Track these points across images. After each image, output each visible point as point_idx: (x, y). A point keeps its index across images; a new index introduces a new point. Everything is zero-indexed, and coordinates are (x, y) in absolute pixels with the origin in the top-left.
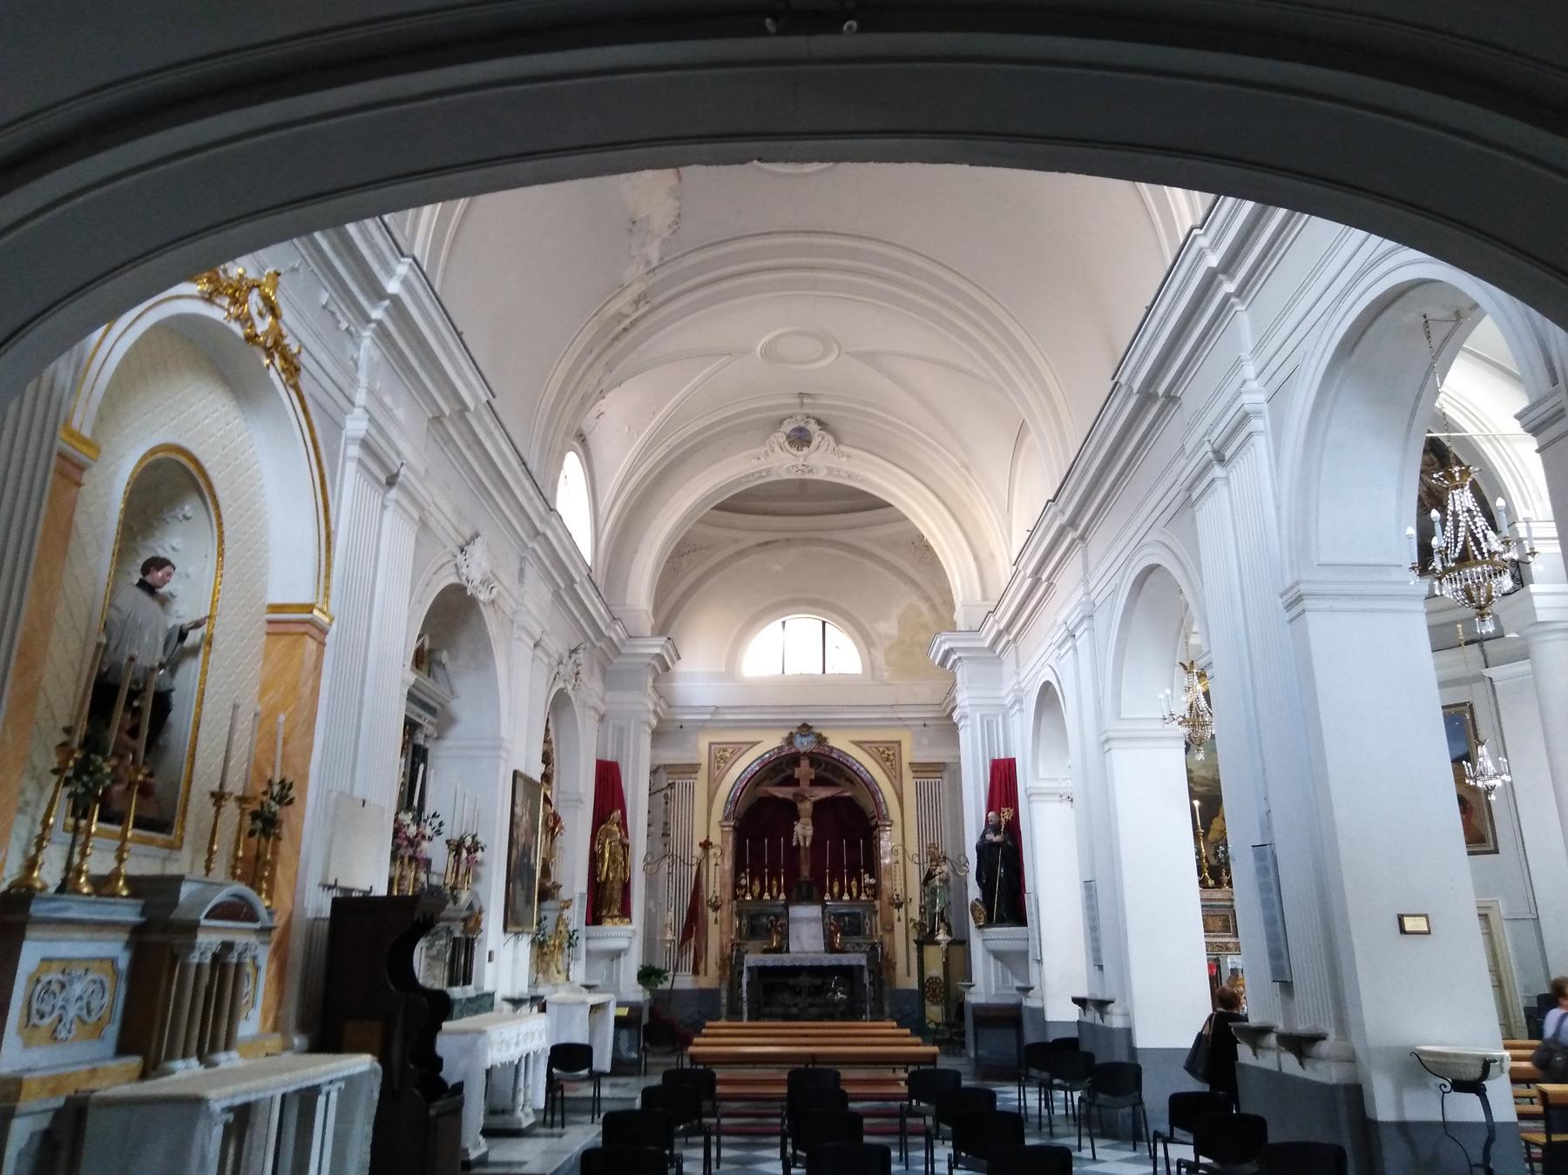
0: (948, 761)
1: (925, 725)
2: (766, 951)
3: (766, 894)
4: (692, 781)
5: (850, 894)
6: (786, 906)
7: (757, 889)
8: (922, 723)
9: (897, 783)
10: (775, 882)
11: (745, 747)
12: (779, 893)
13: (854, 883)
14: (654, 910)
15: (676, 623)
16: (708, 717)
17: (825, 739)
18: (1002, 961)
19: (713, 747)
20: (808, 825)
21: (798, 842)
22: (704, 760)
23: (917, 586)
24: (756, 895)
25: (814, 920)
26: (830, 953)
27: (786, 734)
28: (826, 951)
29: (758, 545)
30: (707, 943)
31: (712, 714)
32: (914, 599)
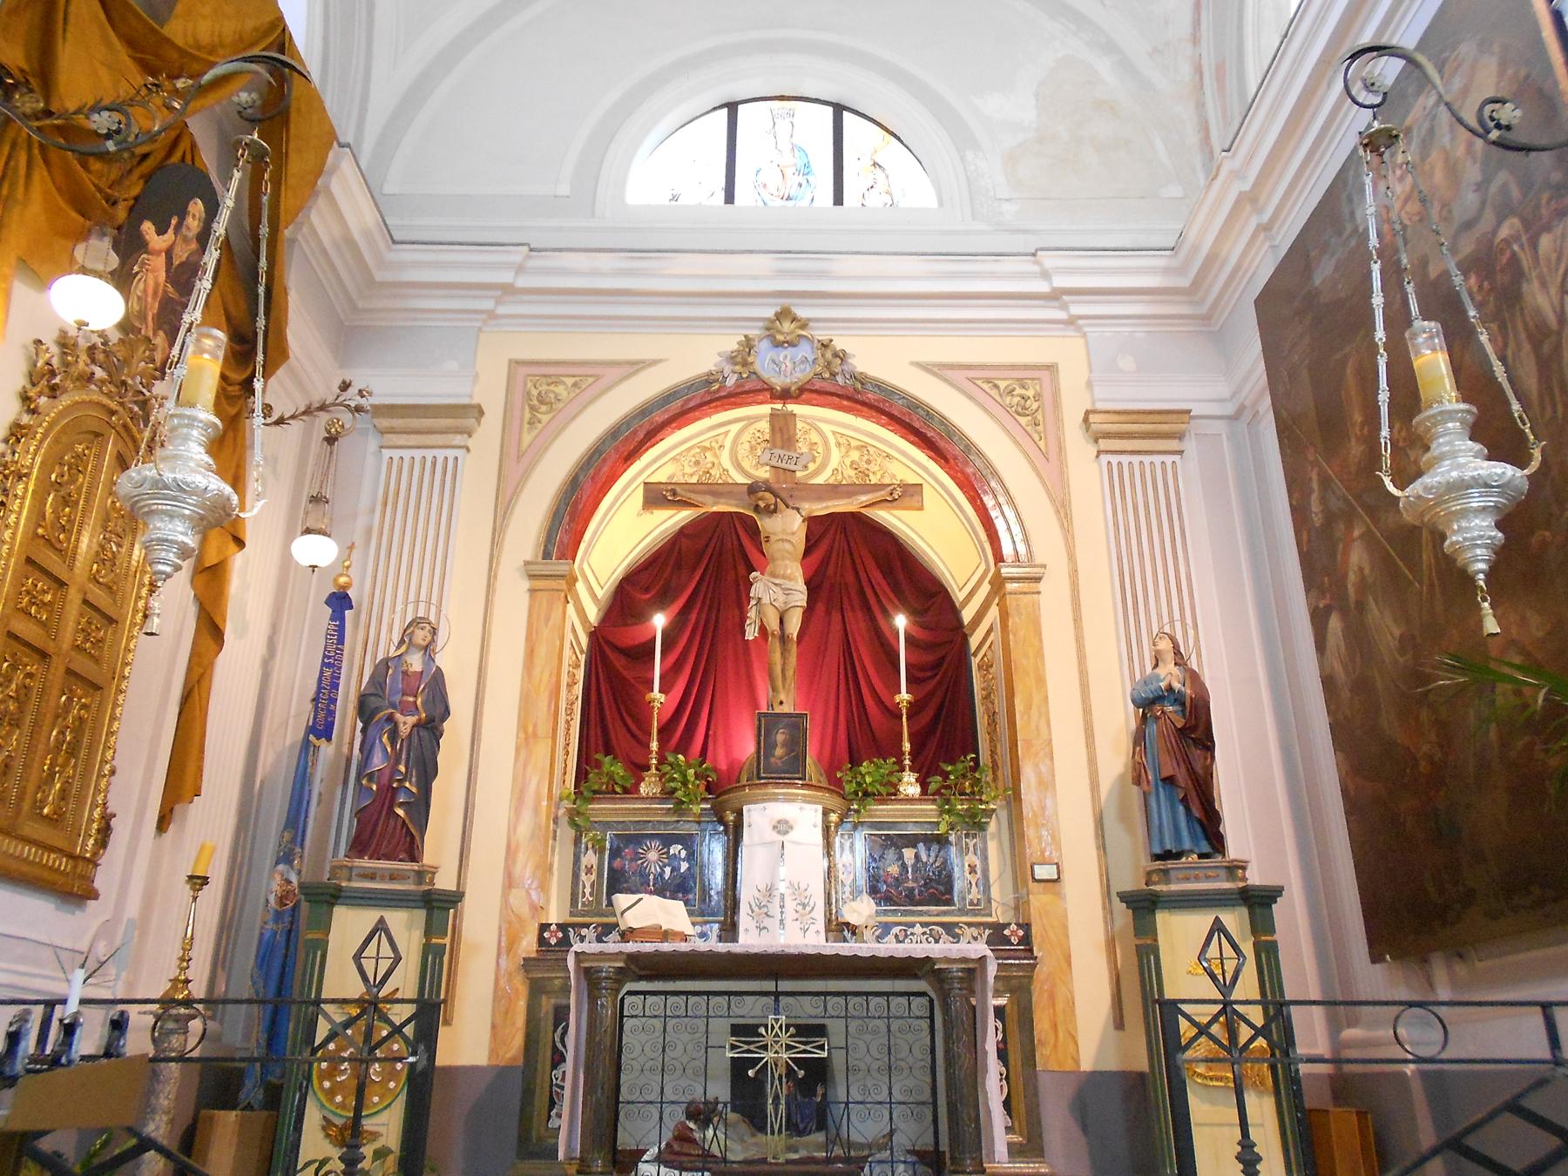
4: (451, 453)
17: (842, 356)
27: (731, 343)
30: (324, 957)
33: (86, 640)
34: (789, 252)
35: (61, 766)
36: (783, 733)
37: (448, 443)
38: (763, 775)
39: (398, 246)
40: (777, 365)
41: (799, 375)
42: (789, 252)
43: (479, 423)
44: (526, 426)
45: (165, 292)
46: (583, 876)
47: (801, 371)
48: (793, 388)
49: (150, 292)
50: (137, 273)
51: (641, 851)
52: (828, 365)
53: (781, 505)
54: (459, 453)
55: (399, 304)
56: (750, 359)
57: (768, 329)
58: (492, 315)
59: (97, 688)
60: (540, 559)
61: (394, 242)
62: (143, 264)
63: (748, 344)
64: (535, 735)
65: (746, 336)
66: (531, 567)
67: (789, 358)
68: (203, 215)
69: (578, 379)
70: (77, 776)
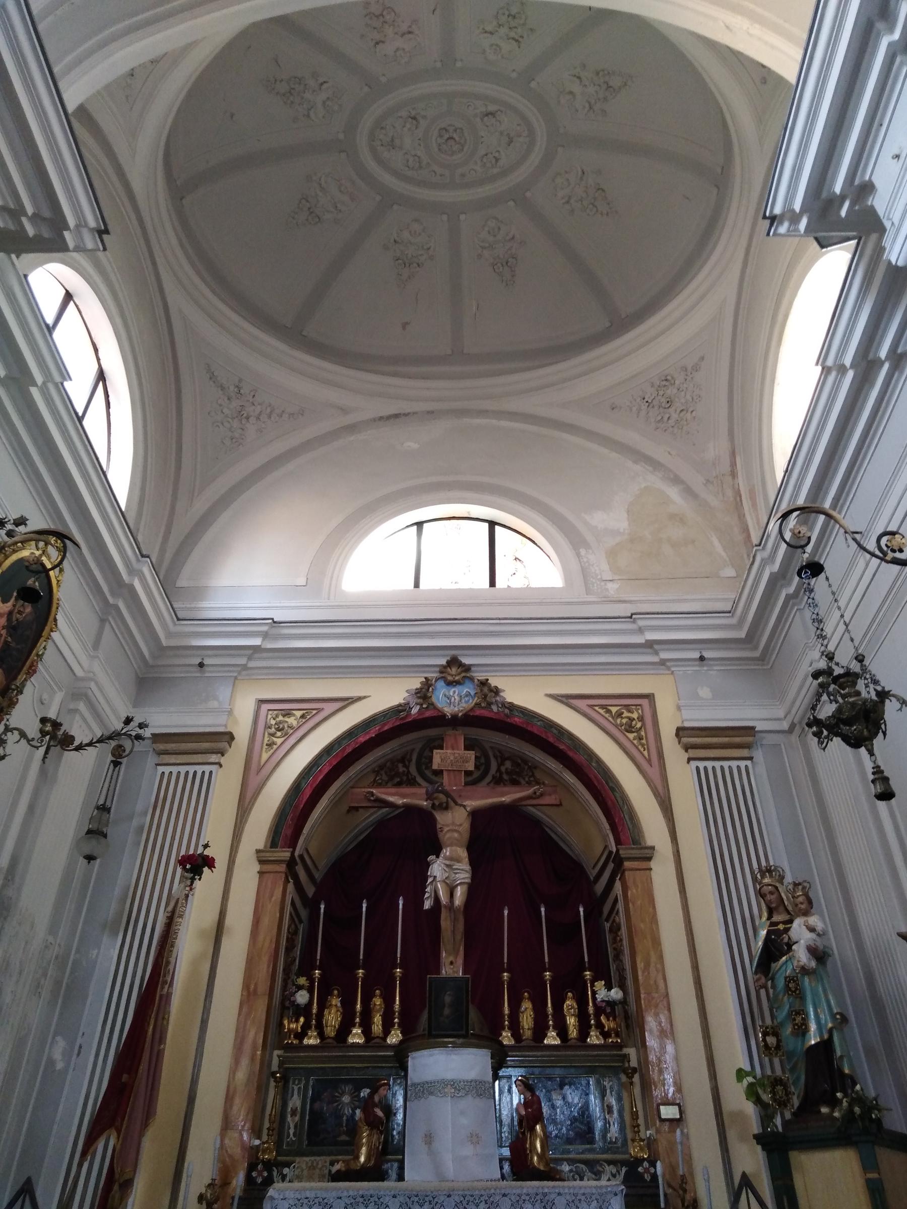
0: (760, 726)
1: (702, 658)
2: (337, 1177)
3: (357, 1031)
4: (207, 769)
5: (562, 1032)
7: (332, 1019)
8: (696, 655)
9: (654, 772)
10: (378, 1001)
11: (329, 708)
12: (387, 1028)
13: (570, 1003)
14: (60, 1066)
15: (224, 517)
16: (257, 641)
17: (496, 691)
19: (265, 707)
20: (459, 860)
21: (437, 899)
22: (242, 732)
23: (655, 464)
24: (330, 1032)
27: (415, 683)
29: (381, 418)
31: (265, 636)
32: (654, 480)
37: (205, 761)
38: (434, 1033)
41: (464, 705)
46: (289, 1119)
47: (466, 702)
48: (460, 714)
51: (337, 1094)
53: (452, 804)
54: (214, 768)
57: (441, 672)
58: (245, 667)
61: (178, 619)
67: (457, 693)
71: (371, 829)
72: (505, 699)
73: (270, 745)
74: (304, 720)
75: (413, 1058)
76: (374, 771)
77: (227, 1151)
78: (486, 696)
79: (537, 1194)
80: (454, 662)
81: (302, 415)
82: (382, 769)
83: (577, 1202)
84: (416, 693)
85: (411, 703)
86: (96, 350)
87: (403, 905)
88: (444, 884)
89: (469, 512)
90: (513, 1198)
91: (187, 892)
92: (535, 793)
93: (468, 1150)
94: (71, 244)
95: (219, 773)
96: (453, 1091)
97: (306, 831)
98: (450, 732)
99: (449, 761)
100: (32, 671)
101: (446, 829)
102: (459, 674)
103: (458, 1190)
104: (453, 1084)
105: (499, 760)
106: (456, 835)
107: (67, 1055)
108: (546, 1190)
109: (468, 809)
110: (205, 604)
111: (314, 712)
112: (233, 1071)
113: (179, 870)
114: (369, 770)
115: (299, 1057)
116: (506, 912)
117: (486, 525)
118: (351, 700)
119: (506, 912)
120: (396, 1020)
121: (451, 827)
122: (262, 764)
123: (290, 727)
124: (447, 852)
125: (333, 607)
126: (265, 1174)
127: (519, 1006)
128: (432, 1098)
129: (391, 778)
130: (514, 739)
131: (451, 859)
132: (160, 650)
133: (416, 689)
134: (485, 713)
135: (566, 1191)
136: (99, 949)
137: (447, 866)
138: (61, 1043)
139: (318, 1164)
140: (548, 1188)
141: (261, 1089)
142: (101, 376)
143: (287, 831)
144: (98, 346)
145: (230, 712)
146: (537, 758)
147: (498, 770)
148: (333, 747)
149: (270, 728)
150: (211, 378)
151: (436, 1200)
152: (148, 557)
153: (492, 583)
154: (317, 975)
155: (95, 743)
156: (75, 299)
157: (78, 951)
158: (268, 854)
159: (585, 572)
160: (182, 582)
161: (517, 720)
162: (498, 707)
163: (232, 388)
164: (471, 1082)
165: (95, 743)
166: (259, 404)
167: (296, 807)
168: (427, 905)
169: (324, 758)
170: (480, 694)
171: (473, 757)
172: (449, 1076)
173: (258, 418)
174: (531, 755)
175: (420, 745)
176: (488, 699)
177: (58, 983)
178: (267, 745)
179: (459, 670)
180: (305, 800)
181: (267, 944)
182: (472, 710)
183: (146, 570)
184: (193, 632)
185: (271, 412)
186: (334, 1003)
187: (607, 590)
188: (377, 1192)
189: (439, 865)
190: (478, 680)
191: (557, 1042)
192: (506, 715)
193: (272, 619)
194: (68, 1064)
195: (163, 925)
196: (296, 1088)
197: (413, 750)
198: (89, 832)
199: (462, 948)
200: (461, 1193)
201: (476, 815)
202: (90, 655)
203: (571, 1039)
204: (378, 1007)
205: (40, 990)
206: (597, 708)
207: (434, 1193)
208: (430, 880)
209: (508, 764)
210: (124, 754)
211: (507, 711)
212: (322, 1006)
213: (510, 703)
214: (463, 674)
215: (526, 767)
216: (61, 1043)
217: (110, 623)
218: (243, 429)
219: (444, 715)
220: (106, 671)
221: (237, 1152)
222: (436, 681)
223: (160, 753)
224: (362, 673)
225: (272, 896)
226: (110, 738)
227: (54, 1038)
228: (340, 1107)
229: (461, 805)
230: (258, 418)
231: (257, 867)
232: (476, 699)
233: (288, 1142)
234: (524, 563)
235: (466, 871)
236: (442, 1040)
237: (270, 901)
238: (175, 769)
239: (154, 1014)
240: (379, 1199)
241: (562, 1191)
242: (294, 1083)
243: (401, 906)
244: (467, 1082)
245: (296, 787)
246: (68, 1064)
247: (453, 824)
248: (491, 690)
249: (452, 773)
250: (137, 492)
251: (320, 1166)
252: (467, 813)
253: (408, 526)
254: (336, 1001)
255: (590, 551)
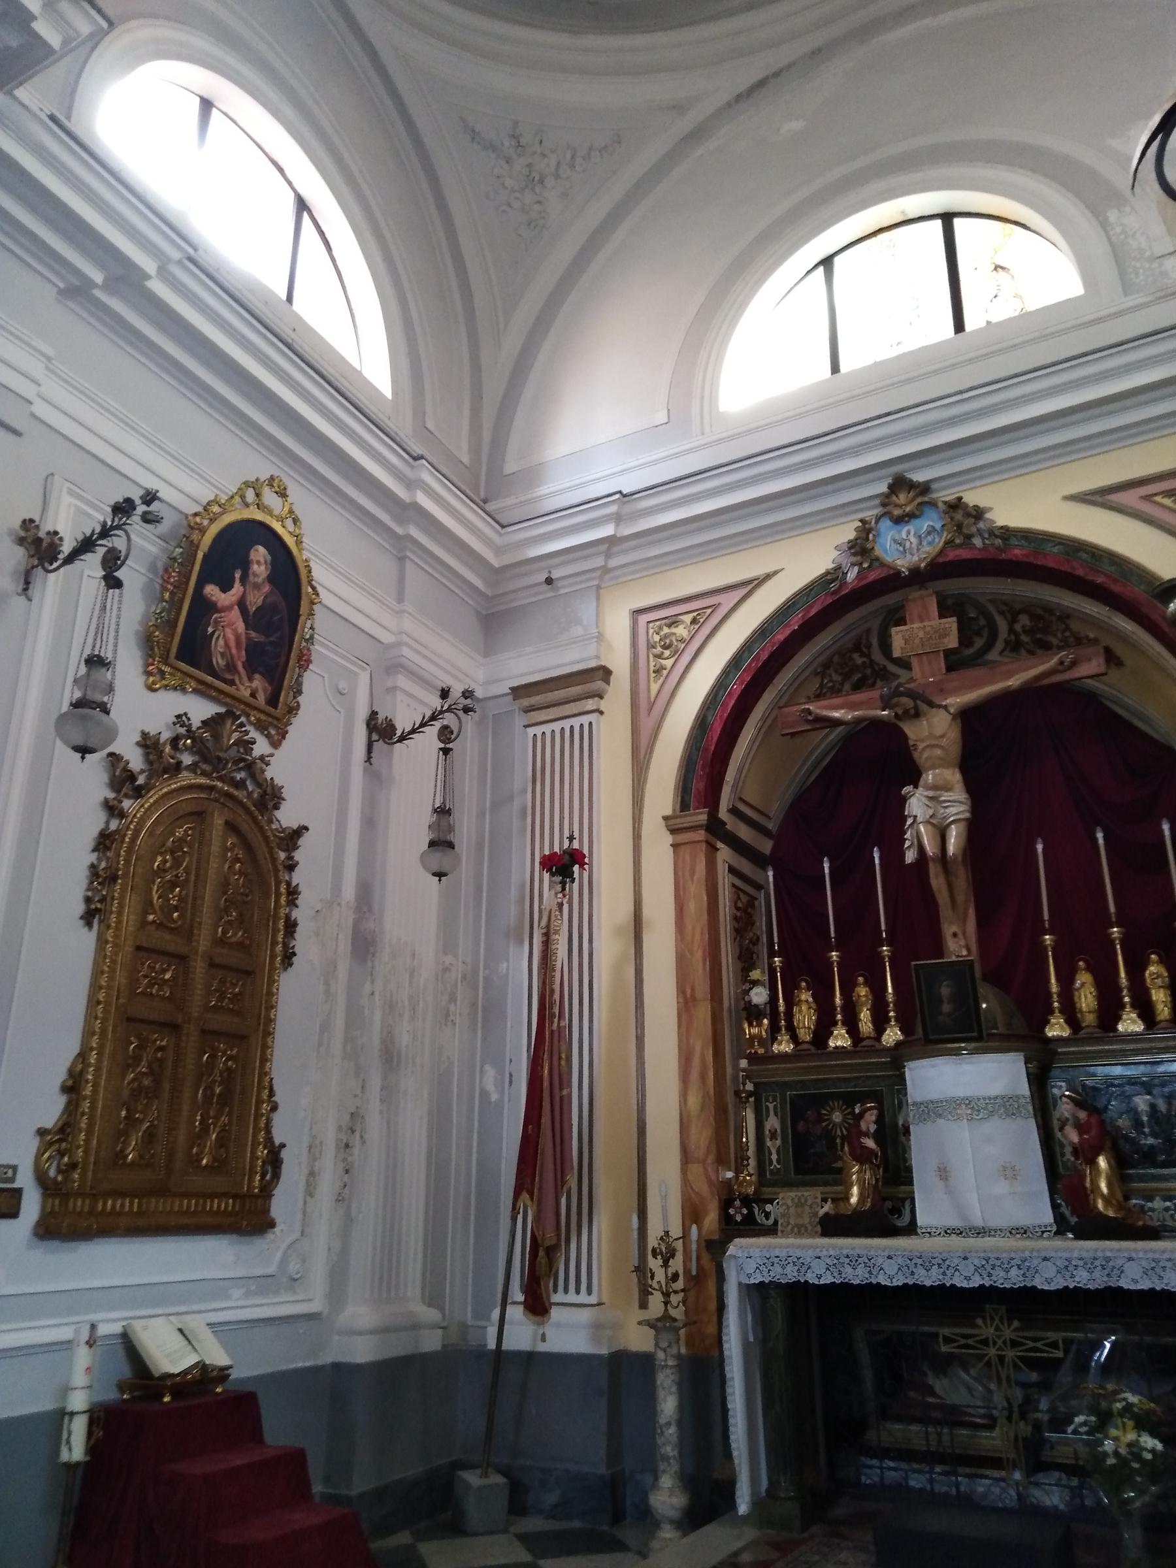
2: (833, 1226)
4: (585, 719)
6: (898, 1057)
7: (806, 1018)
10: (862, 991)
12: (880, 1024)
14: (494, 1097)
16: (608, 530)
17: (978, 514)
18: (106, 708)
19: (643, 619)
20: (947, 788)
21: (921, 849)
22: (619, 661)
24: (805, 1035)
25: (1003, 1106)
26: (1082, 1234)
27: (847, 532)
28: (1062, 1227)
29: (739, 98)
31: (618, 519)
33: (221, 998)
34: (888, 414)
35: (214, 1118)
36: (948, 986)
37: (581, 710)
38: (932, 1037)
39: (509, 529)
40: (900, 544)
41: (927, 549)
42: (888, 414)
43: (608, 683)
44: (653, 675)
45: (248, 639)
46: (769, 1143)
47: (930, 543)
48: (923, 565)
49: (232, 643)
50: (213, 633)
51: (824, 1112)
52: (959, 526)
53: (924, 707)
54: (592, 717)
55: (521, 583)
56: (869, 546)
57: (884, 505)
58: (605, 570)
59: (243, 1038)
60: (678, 813)
61: (503, 527)
62: (216, 623)
63: (866, 530)
64: (694, 999)
65: (861, 521)
66: (671, 822)
67: (912, 533)
68: (269, 558)
69: (695, 614)
70: (235, 1122)
71: (837, 749)
72: (993, 522)
73: (657, 672)
74: (697, 627)
75: (910, 1069)
76: (816, 673)
77: (692, 1188)
78: (959, 526)
79: (1095, 1259)
80: (900, 484)
81: (619, 143)
82: (828, 668)
83: (1158, 1270)
84: (850, 548)
85: (844, 566)
86: (281, 170)
87: (881, 858)
88: (930, 827)
89: (903, 212)
90: (1058, 1263)
91: (560, 900)
92: (1061, 663)
93: (1001, 1188)
94: (54, 40)
95: (602, 725)
96: (969, 1111)
97: (730, 776)
98: (915, 594)
99: (917, 641)
100: (305, 661)
101: (921, 746)
102: (913, 500)
103: (977, 1252)
104: (968, 1102)
105: (1009, 617)
106: (939, 752)
107: (499, 1084)
108: (1108, 1254)
109: (952, 710)
110: (543, 490)
111: (709, 611)
112: (684, 1096)
113: (546, 876)
114: (807, 673)
115: (768, 1070)
116: (1040, 847)
117: (938, 223)
118: (756, 582)
119: (1040, 847)
120: (892, 1014)
121: (928, 743)
122: (652, 700)
123: (682, 640)
124: (929, 777)
125: (720, 441)
126: (745, 1211)
127: (1072, 980)
128: (941, 1121)
129: (846, 677)
130: (1020, 581)
131: (935, 787)
132: (497, 574)
133: (849, 542)
134: (964, 554)
135: (1141, 1255)
136: (508, 961)
137: (931, 798)
138: (490, 1072)
139: (806, 1201)
140: (1111, 1250)
141: (721, 1112)
142: (302, 206)
143: (698, 785)
144: (281, 163)
145: (600, 637)
146: (1066, 603)
147: (1011, 631)
148: (741, 656)
149: (654, 647)
150: (473, 139)
151: (947, 1263)
152: (422, 457)
153: (959, 326)
154: (777, 964)
155: (418, 728)
156: (216, 103)
157: (486, 967)
158: (678, 821)
159: (1119, 255)
160: (510, 467)
161: (1018, 552)
162: (983, 538)
163: (506, 143)
164: (996, 1098)
165: (418, 728)
166: (552, 152)
167: (706, 750)
168: (910, 856)
169: (731, 675)
170: (950, 526)
171: (955, 626)
172: (961, 1092)
173: (557, 176)
174: (1057, 601)
175: (878, 621)
176: (965, 531)
177: (474, 1005)
178: (654, 672)
179: (912, 494)
180: (715, 739)
181: (697, 937)
182: (941, 552)
183: (428, 477)
184: (529, 539)
185: (573, 157)
186: (803, 997)
187: (1165, 274)
188: (865, 1252)
189: (919, 800)
190: (945, 503)
191: (1139, 1027)
192: (998, 548)
193: (620, 492)
194: (502, 1093)
195: (541, 944)
196: (771, 1106)
197: (868, 631)
198: (432, 844)
199: (972, 913)
200: (982, 1255)
201: (968, 717)
202: (392, 610)
203: (1161, 1021)
204: (864, 999)
205: (452, 1017)
206: (1158, 499)
207: (944, 1254)
208: (910, 821)
209: (1024, 620)
210: (453, 737)
211: (998, 542)
212: (790, 1002)
213: (1002, 527)
214: (919, 500)
215: (1054, 619)
216: (490, 1072)
217: (412, 561)
218: (539, 202)
219: (898, 573)
220: (424, 624)
221: (702, 1187)
222: (877, 521)
223: (528, 710)
224: (756, 539)
225: (693, 873)
226: (433, 718)
227: (482, 1067)
228: (830, 1127)
229: (940, 706)
230: (557, 176)
231: (669, 839)
232: (945, 534)
233: (771, 1171)
234: (1012, 271)
235: (961, 802)
236: (944, 1046)
237: (692, 880)
238: (547, 728)
239: (546, 1054)
240: (870, 1260)
241: (1134, 1255)
242: (767, 1100)
243: (877, 861)
244: (990, 1099)
245: (701, 724)
246: (502, 1093)
247: (931, 736)
248: (969, 515)
249: (925, 658)
250: (405, 363)
251: (809, 1203)
252: (950, 717)
253: (809, 272)
254: (806, 996)
255: (1128, 209)
